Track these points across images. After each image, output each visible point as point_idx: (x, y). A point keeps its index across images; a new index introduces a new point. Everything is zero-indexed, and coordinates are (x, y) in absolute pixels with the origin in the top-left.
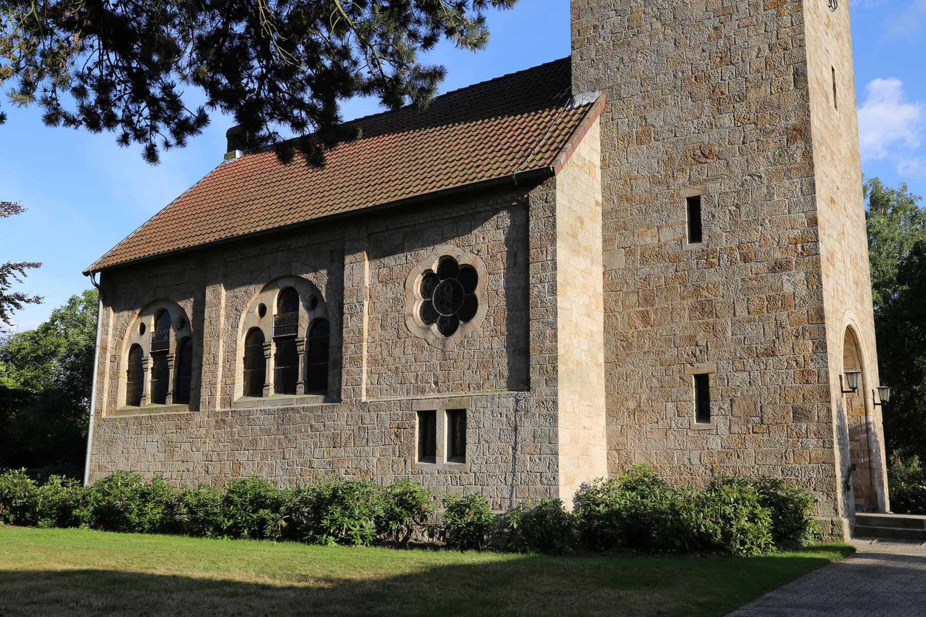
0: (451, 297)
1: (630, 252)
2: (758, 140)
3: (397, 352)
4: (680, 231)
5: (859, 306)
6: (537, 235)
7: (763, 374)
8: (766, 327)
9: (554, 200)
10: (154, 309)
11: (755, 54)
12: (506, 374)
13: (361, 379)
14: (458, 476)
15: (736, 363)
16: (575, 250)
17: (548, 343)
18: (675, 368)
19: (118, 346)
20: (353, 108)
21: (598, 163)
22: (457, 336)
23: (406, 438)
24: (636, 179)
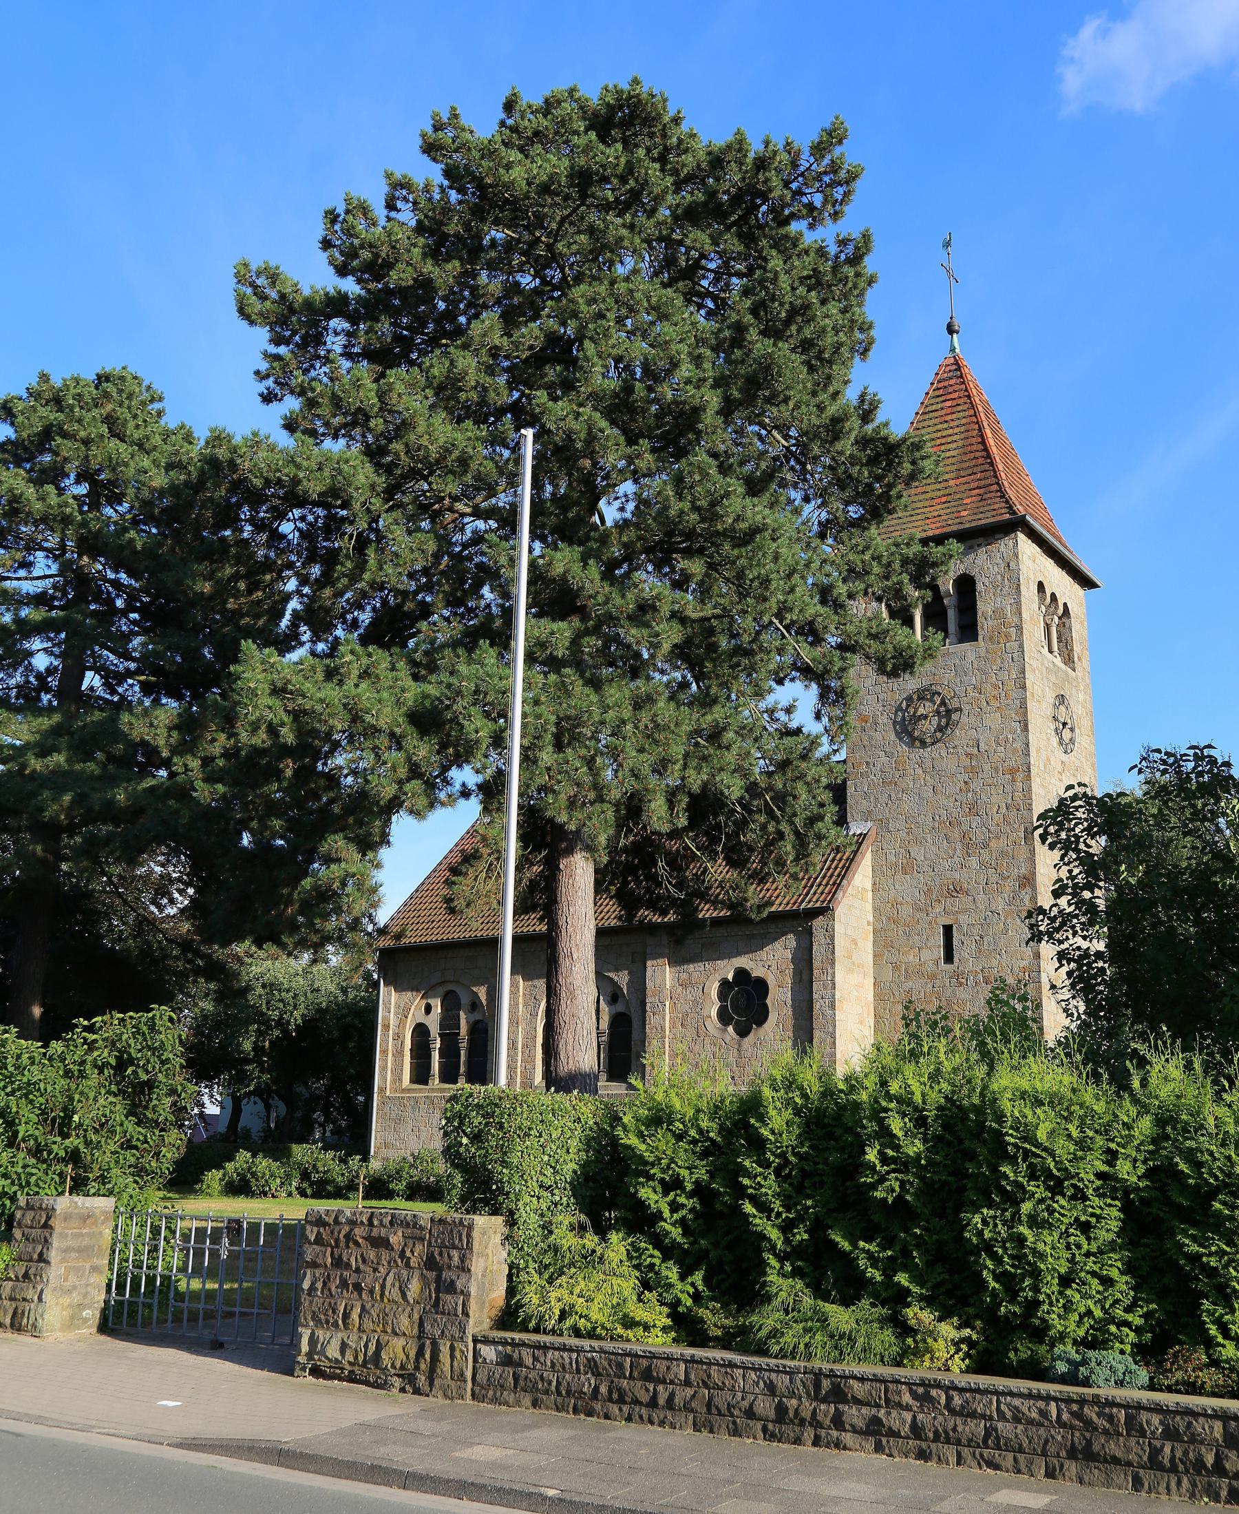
1: (896, 968)
10: (441, 990)
19: (401, 1024)
20: (706, 912)
21: (870, 887)
22: (751, 1038)
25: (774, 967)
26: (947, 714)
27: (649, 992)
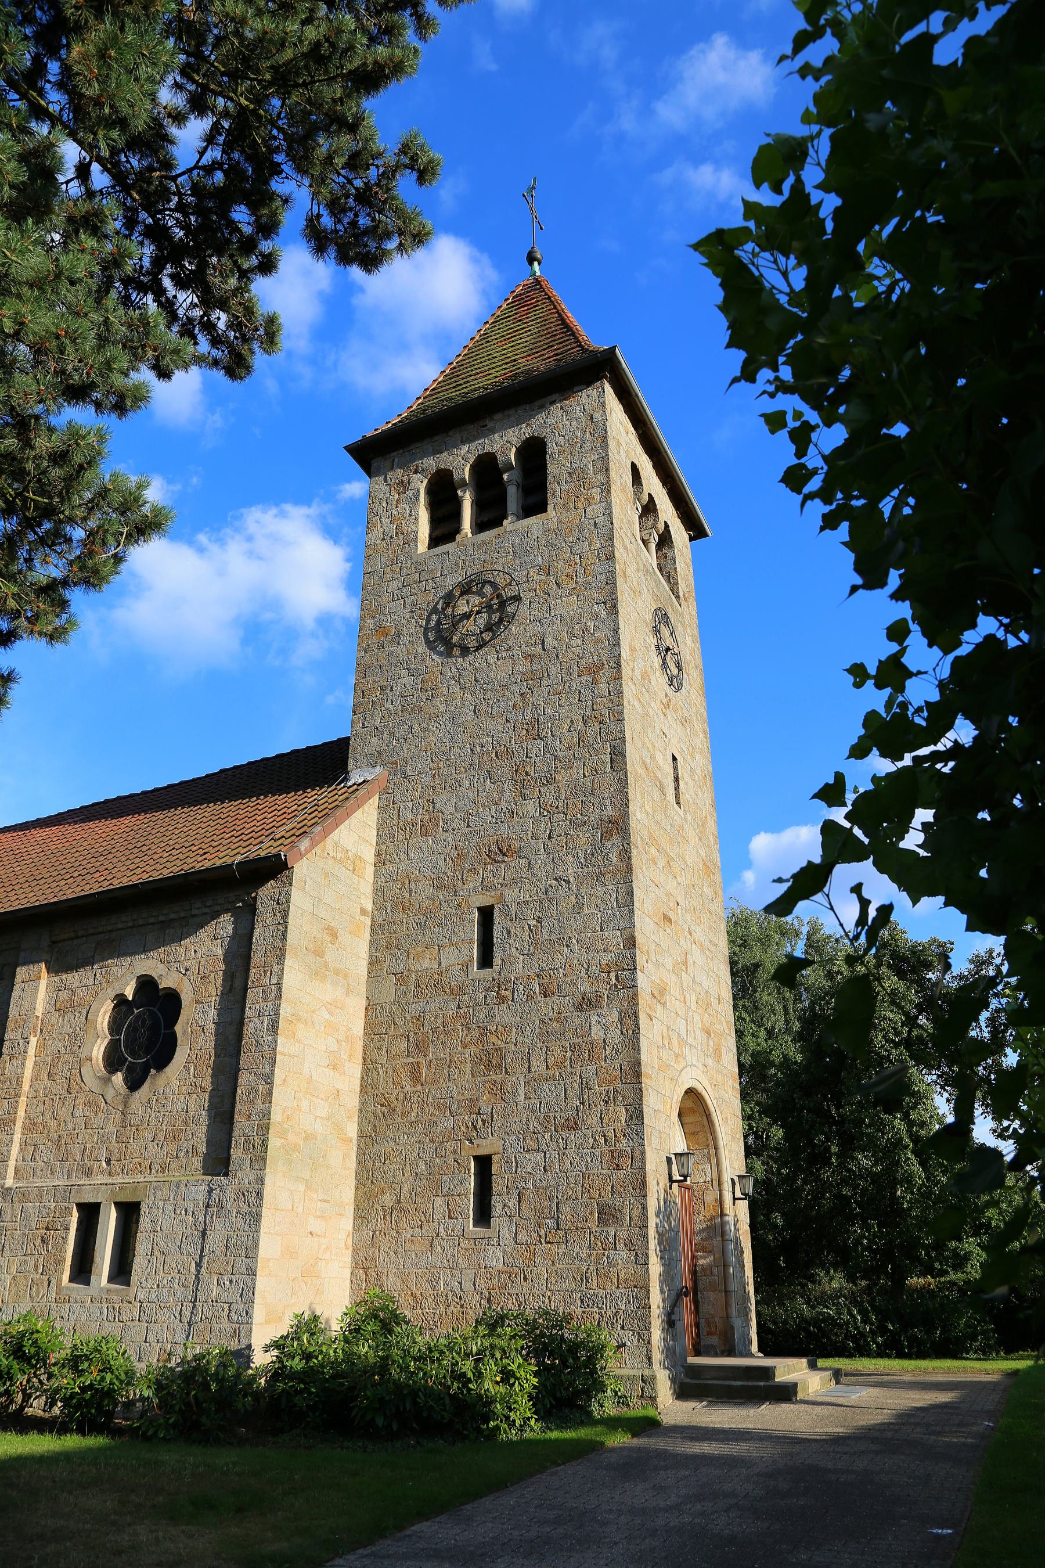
0: (145, 1034)
1: (401, 980)
2: (567, 834)
3: (64, 1112)
4: (467, 952)
5: (710, 1062)
6: (262, 949)
7: (561, 1156)
8: (569, 1088)
9: (288, 901)
11: (566, 727)
12: (202, 1148)
13: (9, 1151)
14: (117, 1306)
15: (528, 1139)
16: (319, 973)
17: (259, 1105)
18: (449, 1145)
21: (370, 858)
23: (55, 1245)
24: (416, 881)
25: (193, 973)
26: (501, 609)
27: (10, 1024)
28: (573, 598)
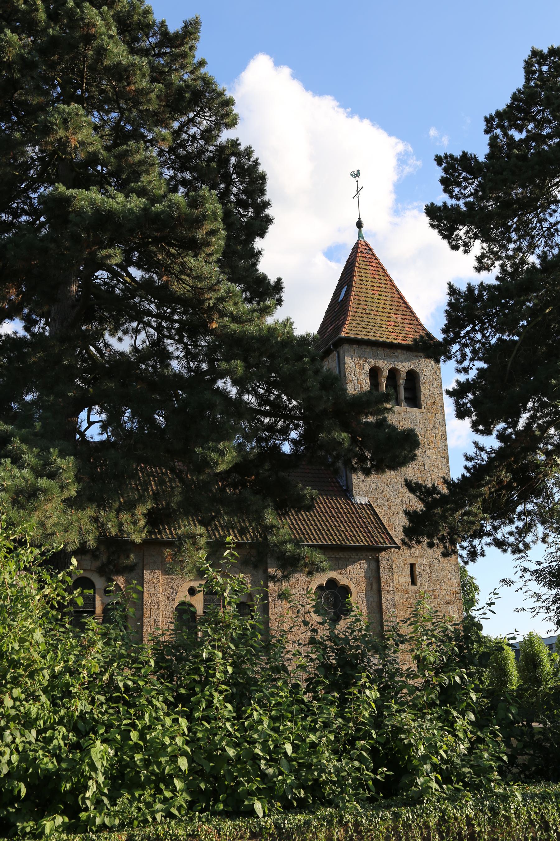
25: (354, 579)
28: (433, 451)
